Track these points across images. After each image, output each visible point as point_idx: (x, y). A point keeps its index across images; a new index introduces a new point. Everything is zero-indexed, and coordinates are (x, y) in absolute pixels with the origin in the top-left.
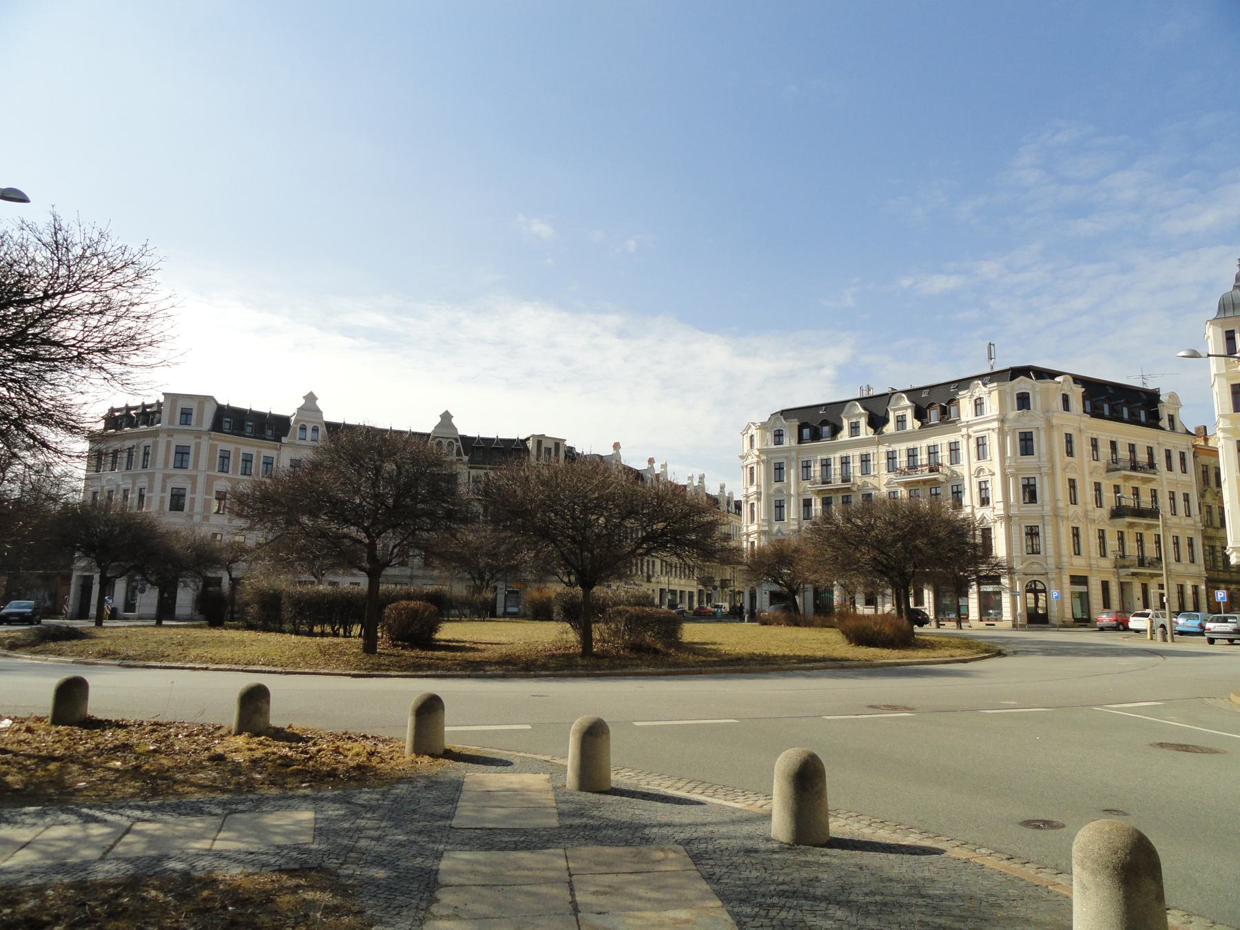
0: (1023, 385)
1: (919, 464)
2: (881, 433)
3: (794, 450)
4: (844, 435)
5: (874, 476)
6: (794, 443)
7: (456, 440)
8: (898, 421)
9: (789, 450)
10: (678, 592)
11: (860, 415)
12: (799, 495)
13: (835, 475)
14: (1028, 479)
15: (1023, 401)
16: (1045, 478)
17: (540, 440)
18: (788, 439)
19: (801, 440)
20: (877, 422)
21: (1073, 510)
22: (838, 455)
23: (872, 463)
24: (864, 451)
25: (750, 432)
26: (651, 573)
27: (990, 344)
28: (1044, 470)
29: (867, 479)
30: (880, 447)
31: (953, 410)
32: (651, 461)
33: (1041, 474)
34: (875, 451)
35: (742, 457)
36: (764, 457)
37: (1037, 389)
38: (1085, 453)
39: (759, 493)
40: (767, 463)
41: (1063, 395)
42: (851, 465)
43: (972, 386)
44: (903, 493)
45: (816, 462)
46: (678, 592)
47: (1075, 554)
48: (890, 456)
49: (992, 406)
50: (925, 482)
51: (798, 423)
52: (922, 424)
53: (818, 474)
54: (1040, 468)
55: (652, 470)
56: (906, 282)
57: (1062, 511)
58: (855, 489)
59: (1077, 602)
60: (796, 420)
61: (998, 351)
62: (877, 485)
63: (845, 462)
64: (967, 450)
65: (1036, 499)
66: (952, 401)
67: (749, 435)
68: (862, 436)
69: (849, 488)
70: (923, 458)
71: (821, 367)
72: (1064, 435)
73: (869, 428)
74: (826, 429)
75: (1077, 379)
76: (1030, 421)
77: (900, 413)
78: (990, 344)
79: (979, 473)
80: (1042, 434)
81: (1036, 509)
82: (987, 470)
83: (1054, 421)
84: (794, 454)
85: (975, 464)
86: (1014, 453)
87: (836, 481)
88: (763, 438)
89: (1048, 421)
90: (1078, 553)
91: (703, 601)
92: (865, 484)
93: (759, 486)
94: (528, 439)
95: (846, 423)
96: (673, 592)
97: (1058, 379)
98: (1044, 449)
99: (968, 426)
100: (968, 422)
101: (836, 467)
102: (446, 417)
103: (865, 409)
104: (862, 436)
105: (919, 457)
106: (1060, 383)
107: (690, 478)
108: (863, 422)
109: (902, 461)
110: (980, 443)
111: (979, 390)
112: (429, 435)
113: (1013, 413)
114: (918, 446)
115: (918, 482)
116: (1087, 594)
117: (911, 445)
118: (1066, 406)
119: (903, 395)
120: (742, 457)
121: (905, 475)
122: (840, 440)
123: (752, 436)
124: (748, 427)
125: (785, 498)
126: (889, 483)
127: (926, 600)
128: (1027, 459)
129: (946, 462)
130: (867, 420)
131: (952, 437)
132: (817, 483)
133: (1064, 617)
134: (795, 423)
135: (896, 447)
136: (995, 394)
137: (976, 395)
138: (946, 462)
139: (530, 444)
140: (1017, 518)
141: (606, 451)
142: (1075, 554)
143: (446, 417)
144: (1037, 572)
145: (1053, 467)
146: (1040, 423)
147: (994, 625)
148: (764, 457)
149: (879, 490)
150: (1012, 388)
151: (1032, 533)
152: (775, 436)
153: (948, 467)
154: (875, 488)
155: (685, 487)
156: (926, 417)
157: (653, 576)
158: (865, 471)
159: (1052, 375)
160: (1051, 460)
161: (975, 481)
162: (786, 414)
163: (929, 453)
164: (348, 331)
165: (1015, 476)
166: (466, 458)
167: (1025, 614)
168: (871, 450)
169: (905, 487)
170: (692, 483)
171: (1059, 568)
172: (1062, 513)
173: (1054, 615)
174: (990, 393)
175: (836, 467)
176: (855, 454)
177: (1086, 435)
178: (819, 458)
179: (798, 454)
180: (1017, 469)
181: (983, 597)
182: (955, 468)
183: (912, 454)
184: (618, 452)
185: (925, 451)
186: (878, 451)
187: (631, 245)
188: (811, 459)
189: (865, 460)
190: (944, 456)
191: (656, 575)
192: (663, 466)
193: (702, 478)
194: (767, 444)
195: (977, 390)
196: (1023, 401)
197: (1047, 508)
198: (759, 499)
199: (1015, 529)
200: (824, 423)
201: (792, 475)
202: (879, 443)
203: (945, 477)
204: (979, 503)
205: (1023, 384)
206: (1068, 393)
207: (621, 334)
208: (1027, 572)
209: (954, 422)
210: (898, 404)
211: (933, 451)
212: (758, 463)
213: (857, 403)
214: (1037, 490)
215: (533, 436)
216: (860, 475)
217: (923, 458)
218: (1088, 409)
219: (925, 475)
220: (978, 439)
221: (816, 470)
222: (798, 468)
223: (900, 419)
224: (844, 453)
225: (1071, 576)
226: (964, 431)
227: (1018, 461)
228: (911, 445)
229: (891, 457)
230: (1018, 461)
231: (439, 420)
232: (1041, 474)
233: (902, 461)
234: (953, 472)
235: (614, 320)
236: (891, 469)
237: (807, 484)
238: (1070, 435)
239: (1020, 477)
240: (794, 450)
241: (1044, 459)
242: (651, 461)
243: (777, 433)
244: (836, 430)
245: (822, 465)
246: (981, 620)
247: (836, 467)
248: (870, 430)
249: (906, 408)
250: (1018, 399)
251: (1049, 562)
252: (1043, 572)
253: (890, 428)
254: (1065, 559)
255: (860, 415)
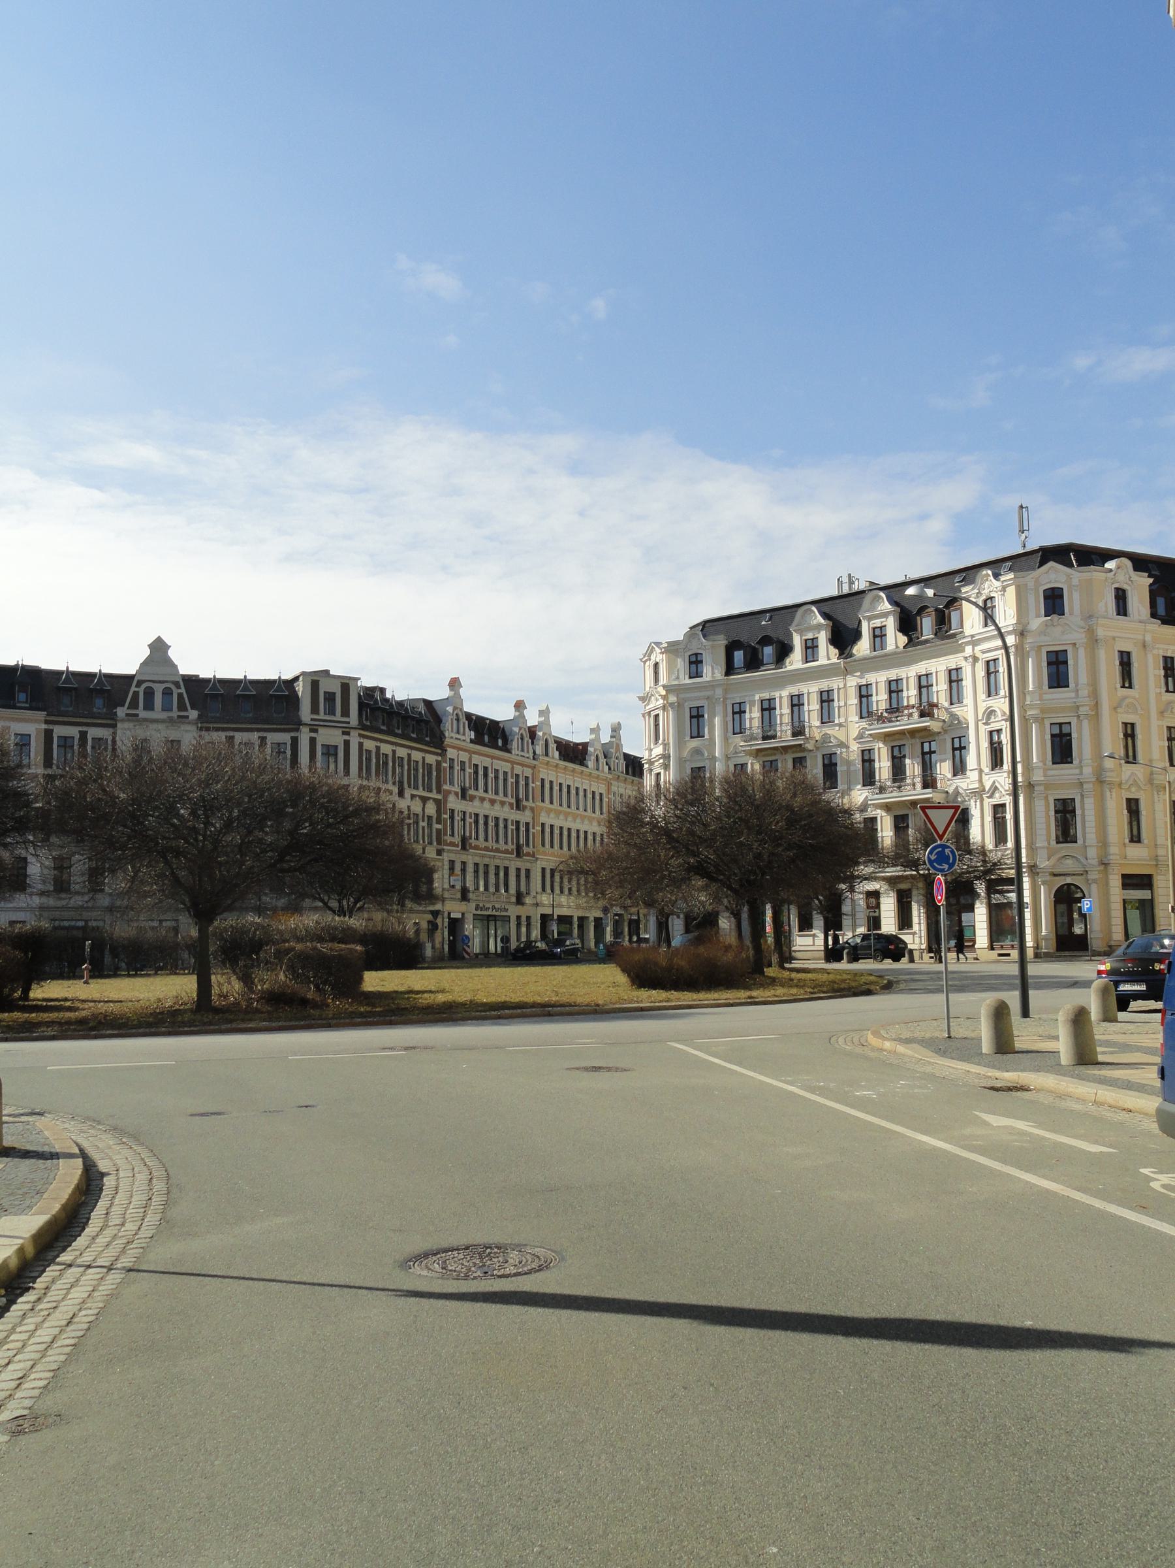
0: (1053, 576)
1: (905, 704)
2: (851, 655)
3: (719, 685)
4: (795, 661)
5: (840, 725)
6: (719, 674)
7: (177, 684)
8: (807, 648)
9: (711, 686)
10: (575, 919)
11: (818, 627)
12: (728, 758)
13: (781, 724)
14: (1060, 724)
15: (1054, 601)
16: (1085, 724)
17: (316, 680)
18: (710, 668)
19: (730, 669)
20: (843, 638)
21: (1128, 773)
22: (785, 693)
23: (836, 704)
24: (824, 684)
25: (653, 657)
26: (523, 889)
27: (1021, 507)
28: (1083, 710)
29: (830, 730)
30: (849, 678)
31: (954, 616)
32: (519, 706)
33: (1078, 717)
34: (841, 685)
35: (642, 699)
36: (673, 699)
37: (1075, 582)
38: (1152, 684)
39: (666, 757)
40: (678, 707)
41: (1117, 589)
42: (806, 708)
43: (978, 579)
44: (754, 767)
45: (752, 703)
46: (575, 919)
47: (1132, 841)
48: (825, 697)
49: (1007, 614)
50: (913, 733)
51: (726, 642)
52: (910, 640)
53: (756, 723)
54: (1078, 707)
55: (521, 720)
56: (1082, 362)
57: (1108, 774)
58: (809, 746)
59: (1134, 916)
60: (722, 637)
61: (1034, 524)
62: (844, 740)
63: (797, 703)
64: (973, 680)
65: (1071, 755)
66: (953, 602)
67: (652, 662)
68: (822, 661)
69: (800, 745)
70: (910, 694)
71: (924, 517)
72: (1117, 655)
73: (831, 648)
74: (768, 651)
75: (1141, 562)
76: (1063, 633)
77: (877, 623)
78: (1021, 507)
79: (989, 718)
80: (1082, 652)
81: (1071, 772)
82: (999, 713)
83: (1101, 633)
84: (719, 692)
85: (984, 703)
86: (1039, 686)
87: (784, 734)
88: (670, 670)
89: (1091, 633)
90: (1136, 838)
91: (622, 933)
92: (826, 738)
93: (665, 745)
94: (296, 679)
95: (797, 641)
96: (564, 920)
97: (1110, 565)
98: (1083, 678)
99: (974, 643)
100: (972, 636)
101: (783, 711)
102: (159, 648)
103: (826, 616)
104: (822, 661)
105: (905, 694)
106: (1111, 570)
107: (595, 730)
108: (823, 637)
109: (880, 700)
110: (924, 683)
111: (989, 585)
112: (128, 679)
113: (1037, 621)
114: (904, 676)
115: (902, 733)
116: (1152, 901)
117: (893, 674)
118: (1122, 608)
119: (882, 594)
120: (642, 699)
121: (884, 722)
122: (789, 668)
123: (656, 665)
124: (650, 651)
125: (707, 764)
126: (860, 736)
127: (915, 920)
128: (1060, 694)
129: (943, 701)
130: (829, 636)
131: (952, 661)
132: (756, 739)
133: (1110, 939)
134: (721, 642)
135: (871, 678)
136: (1012, 591)
137: (985, 593)
138: (943, 701)
139: (300, 687)
140: (1042, 788)
141: (437, 692)
142: (1132, 841)
143: (159, 648)
144: (1071, 870)
145: (1097, 706)
146: (1079, 637)
147: (1008, 955)
148: (673, 699)
149: (847, 747)
150: (1037, 580)
151: (1065, 813)
152: (691, 663)
153: (946, 709)
154: (842, 745)
155: (585, 745)
156: (916, 630)
157: (528, 893)
158: (826, 717)
159: (1103, 555)
160: (1095, 694)
161: (984, 730)
162: (708, 627)
163: (920, 687)
164: (91, 477)
165: (1039, 720)
166: (193, 714)
167: (1053, 936)
168: (834, 683)
169: (884, 742)
170: (598, 739)
171: (1105, 864)
172: (1110, 777)
173: (1096, 940)
174: (1004, 589)
175: (754, 715)
176: (811, 690)
177: (1155, 652)
178: (757, 697)
179: (726, 691)
180: (1043, 711)
181: (995, 911)
182: (957, 710)
183: (894, 689)
184: (457, 696)
185: (913, 683)
186: (845, 685)
187: (599, 306)
188: (747, 699)
189: (826, 699)
190: (940, 690)
191: (533, 893)
192: (541, 713)
193: (616, 730)
194: (678, 678)
195: (987, 584)
196: (1054, 601)
197: (1088, 771)
198: (666, 767)
199: (1040, 805)
200: (766, 641)
201: (717, 725)
202: (847, 672)
203: (940, 724)
204: (989, 764)
205: (1054, 574)
206: (1125, 587)
207: (576, 468)
208: (1057, 871)
209: (954, 636)
210: (874, 608)
211: (923, 683)
212: (664, 708)
213: (814, 608)
214: (1073, 740)
215: (303, 673)
216: (818, 723)
217: (910, 694)
218: (1161, 610)
219: (913, 722)
220: (988, 662)
221: (753, 716)
222: (726, 715)
223: (878, 632)
224: (794, 689)
225: (1124, 876)
226: (968, 650)
227: (1046, 697)
228: (893, 674)
229: (864, 694)
230: (1046, 697)
231: (147, 652)
232: (1078, 717)
233: (880, 700)
234: (953, 716)
235: (567, 443)
236: (865, 714)
237: (738, 741)
238: (1128, 653)
239: (1047, 723)
240: (719, 685)
241: (1084, 692)
242: (519, 706)
243: (693, 659)
244: (784, 651)
245: (763, 710)
246: (992, 949)
247: (783, 711)
248: (834, 651)
249: (885, 615)
250: (1046, 598)
251: (1089, 856)
252: (1080, 870)
253: (863, 648)
254: (1114, 850)
255: (818, 627)
